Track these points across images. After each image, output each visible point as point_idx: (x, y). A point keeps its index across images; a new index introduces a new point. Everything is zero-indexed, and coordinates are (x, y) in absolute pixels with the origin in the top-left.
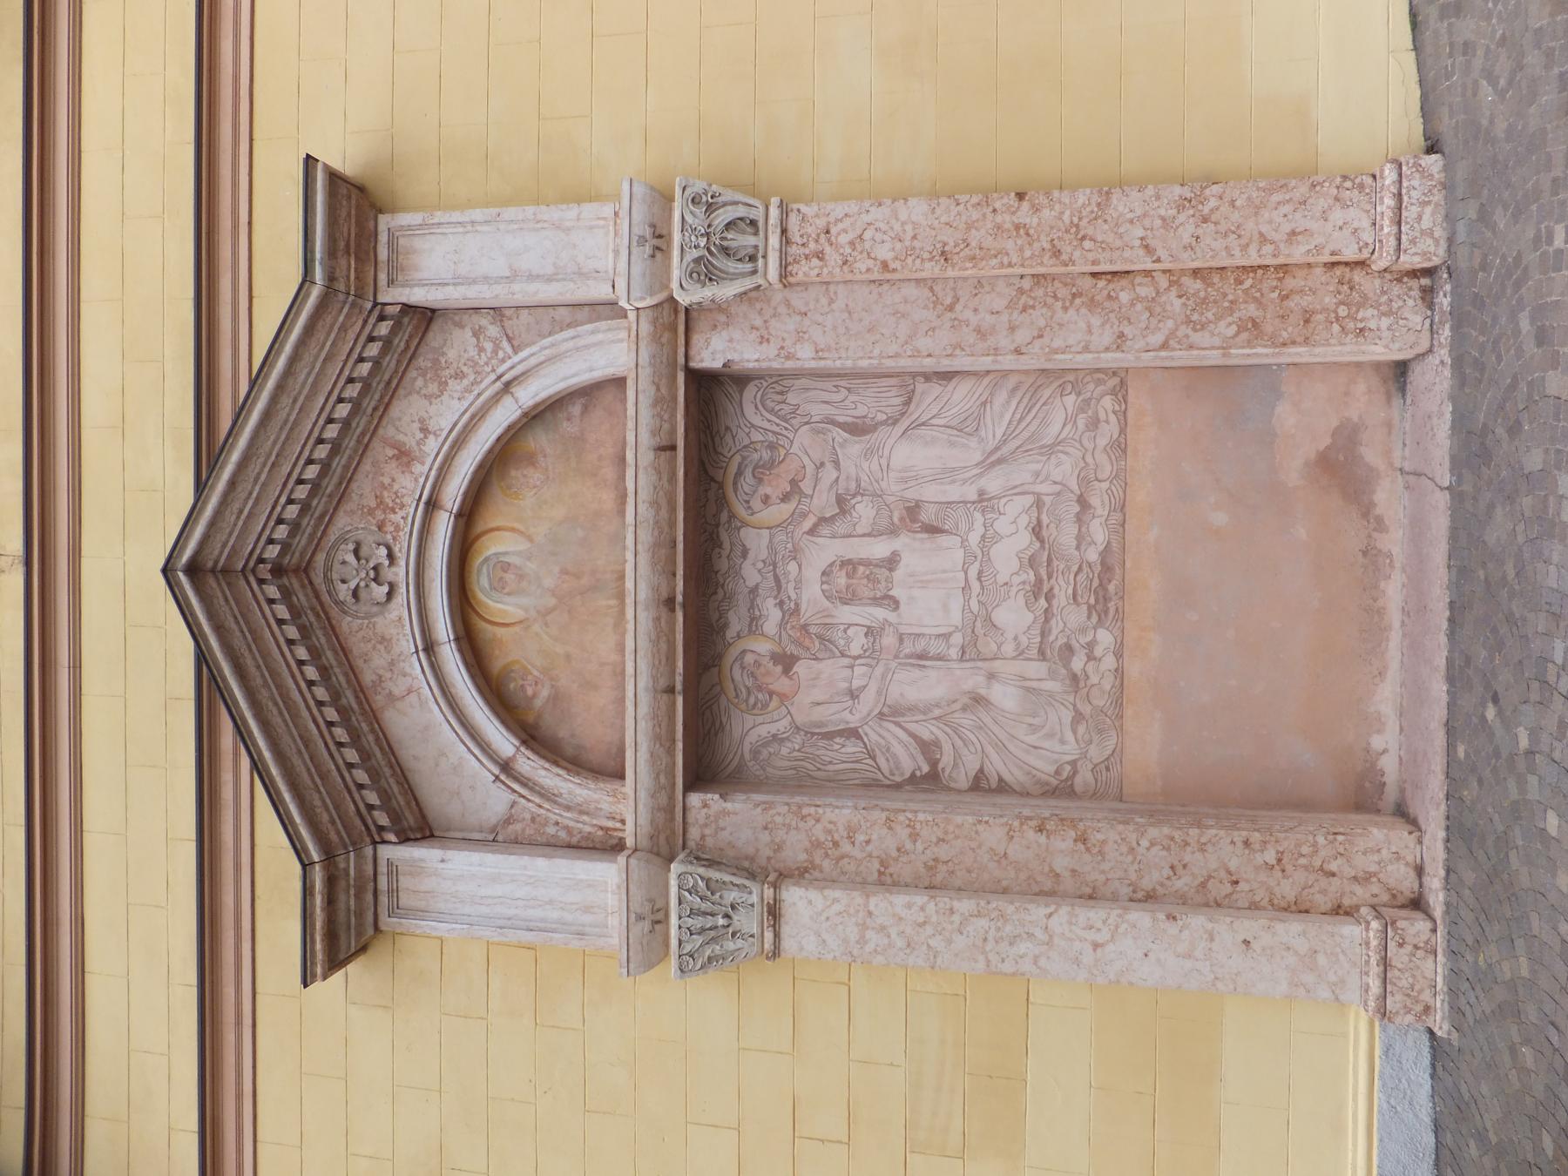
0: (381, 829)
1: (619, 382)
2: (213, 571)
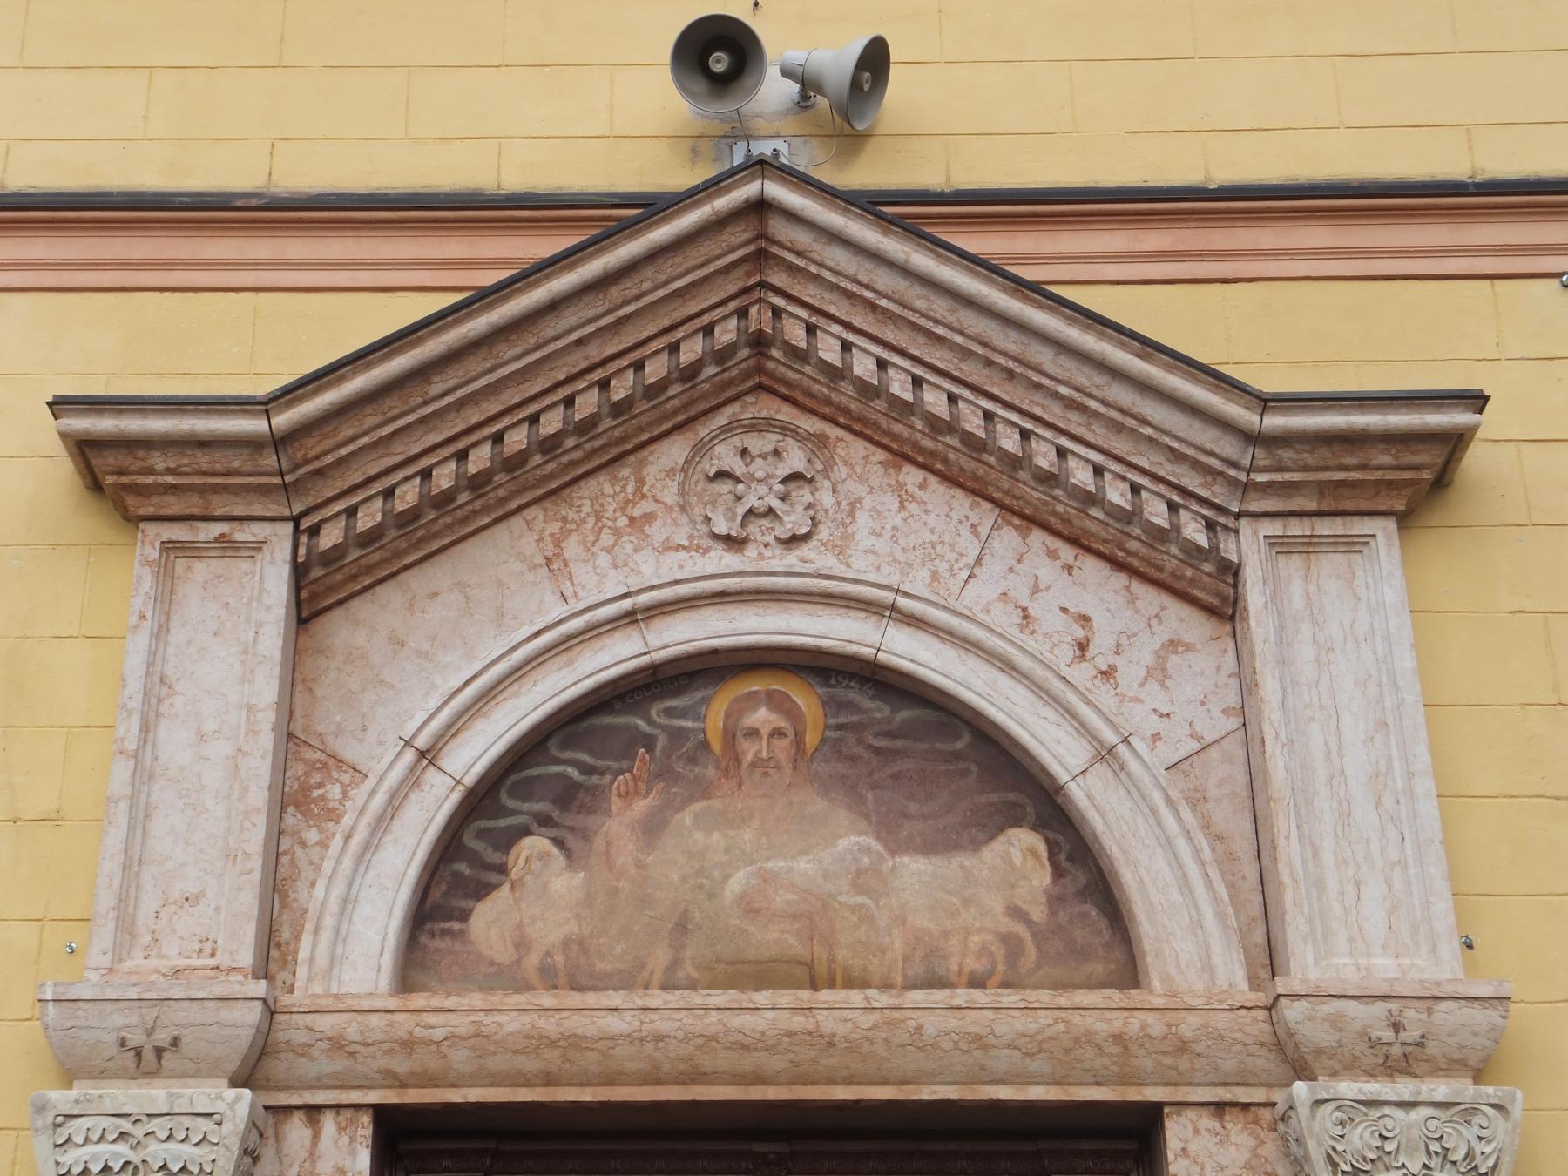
0: (314, 531)
1: (1130, 974)
2: (763, 236)
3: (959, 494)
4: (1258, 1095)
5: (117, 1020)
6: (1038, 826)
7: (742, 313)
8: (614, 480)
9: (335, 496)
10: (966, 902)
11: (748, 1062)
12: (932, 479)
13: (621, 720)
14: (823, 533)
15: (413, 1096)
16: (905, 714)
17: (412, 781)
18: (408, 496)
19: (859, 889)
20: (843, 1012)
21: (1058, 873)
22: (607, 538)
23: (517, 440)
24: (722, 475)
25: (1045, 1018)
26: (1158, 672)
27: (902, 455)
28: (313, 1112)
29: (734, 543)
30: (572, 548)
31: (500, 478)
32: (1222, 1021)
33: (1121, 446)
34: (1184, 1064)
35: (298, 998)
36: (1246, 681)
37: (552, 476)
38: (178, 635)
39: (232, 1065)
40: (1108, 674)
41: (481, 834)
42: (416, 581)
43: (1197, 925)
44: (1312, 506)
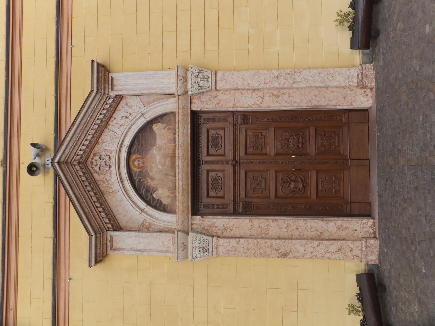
0: (109, 228)
3: (103, 134)
4: (189, 98)
5: (180, 251)
6: (152, 125)
7: (75, 165)
8: (100, 184)
9: (103, 225)
10: (163, 135)
11: (186, 165)
12: (101, 138)
13: (136, 183)
14: (109, 154)
15: (190, 211)
16: (136, 143)
17: (146, 213)
18: (103, 215)
19: (161, 150)
20: (179, 152)
21: (159, 122)
22: (109, 185)
23: (95, 199)
24: (99, 169)
25: (180, 125)
26: (130, 107)
27: (97, 142)
28: (192, 224)
29: (110, 167)
30: (111, 191)
31: (100, 201)
32: (180, 102)
33: (97, 111)
34: (186, 107)
35: (177, 227)
36: (131, 95)
37: (100, 194)
38: (124, 247)
39: (186, 235)
40: (131, 114)
41: (153, 203)
42: (115, 213)
43: (167, 104)
44: (107, 84)
